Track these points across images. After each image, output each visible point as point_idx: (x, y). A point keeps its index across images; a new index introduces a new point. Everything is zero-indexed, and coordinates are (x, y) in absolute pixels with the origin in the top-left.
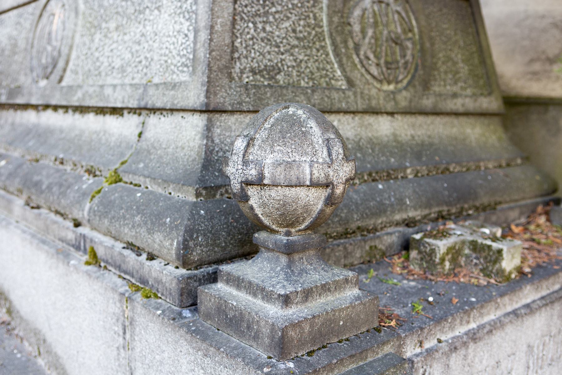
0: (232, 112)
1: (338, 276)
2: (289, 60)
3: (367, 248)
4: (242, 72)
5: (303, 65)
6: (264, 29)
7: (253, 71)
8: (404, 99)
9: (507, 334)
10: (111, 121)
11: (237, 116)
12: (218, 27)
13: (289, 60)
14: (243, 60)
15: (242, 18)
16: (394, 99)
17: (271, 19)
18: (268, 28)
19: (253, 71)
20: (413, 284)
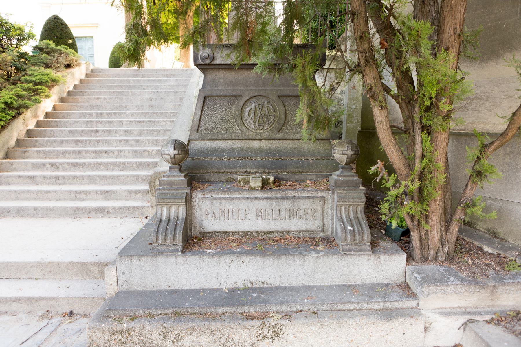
0: (197, 140)
1: (291, 109)
2: (218, 126)
3: (227, 177)
4: (202, 130)
5: (224, 127)
6: (211, 119)
7: (205, 130)
8: (265, 135)
9: (244, 284)
10: (242, 104)
11: (199, 141)
12: (195, 120)
13: (218, 126)
14: (203, 127)
15: (204, 116)
16: (261, 135)
17: (214, 115)
18: (212, 118)
19: (205, 130)
20: (371, 25)
